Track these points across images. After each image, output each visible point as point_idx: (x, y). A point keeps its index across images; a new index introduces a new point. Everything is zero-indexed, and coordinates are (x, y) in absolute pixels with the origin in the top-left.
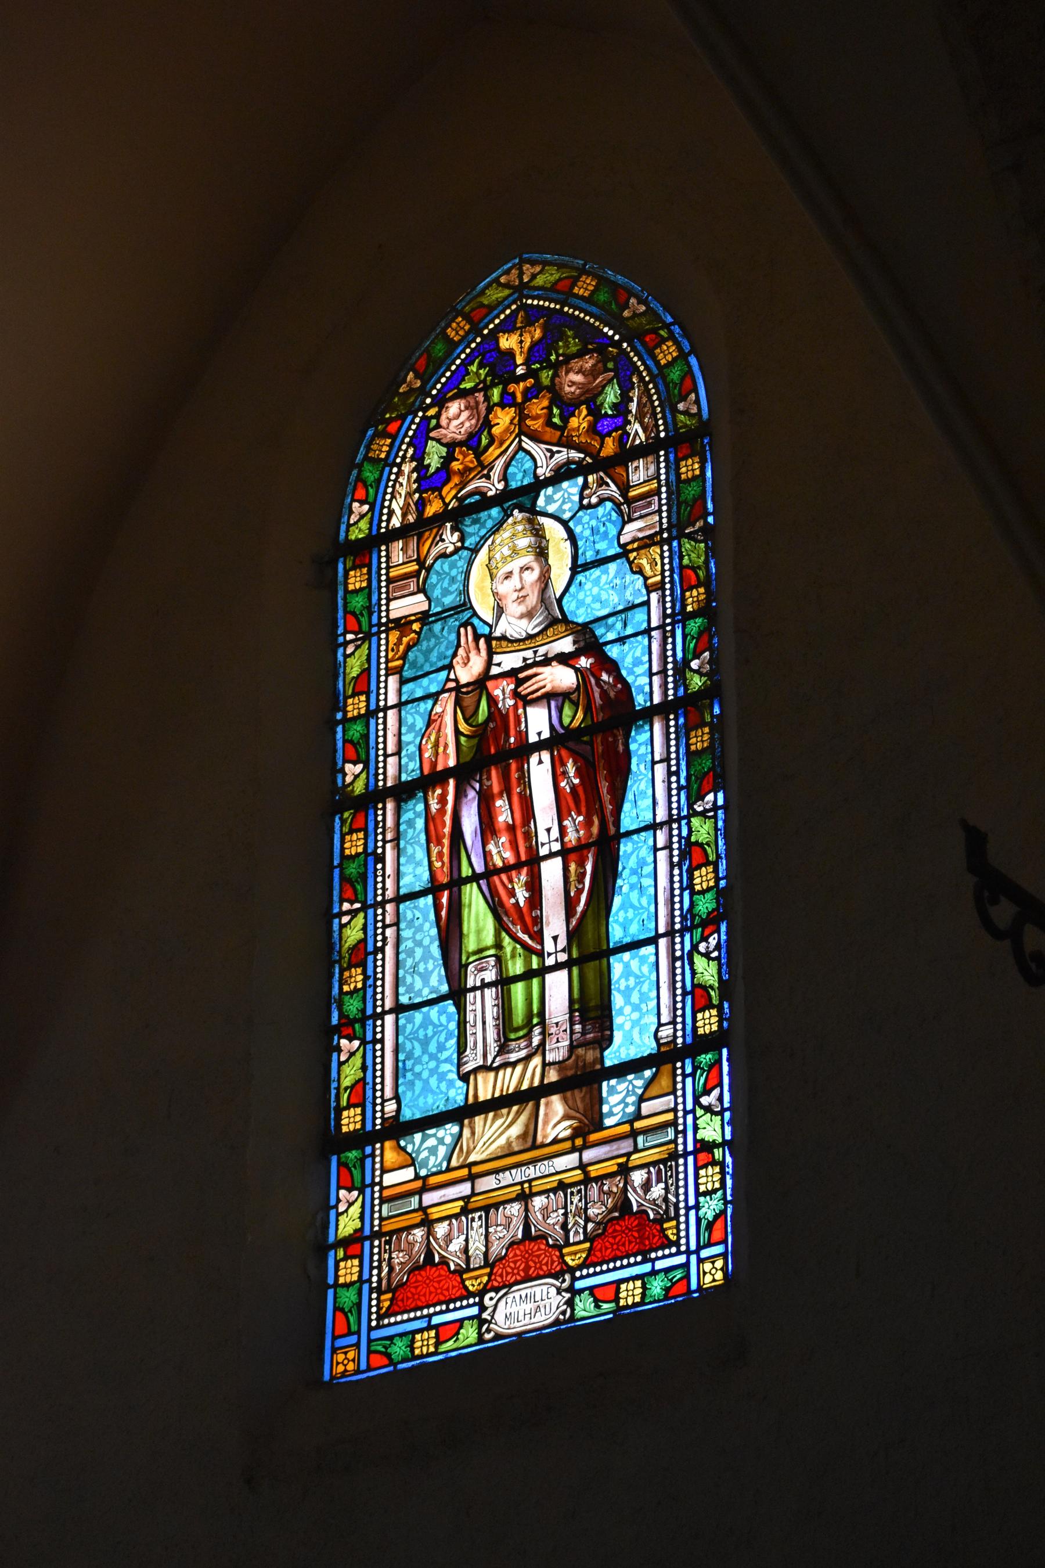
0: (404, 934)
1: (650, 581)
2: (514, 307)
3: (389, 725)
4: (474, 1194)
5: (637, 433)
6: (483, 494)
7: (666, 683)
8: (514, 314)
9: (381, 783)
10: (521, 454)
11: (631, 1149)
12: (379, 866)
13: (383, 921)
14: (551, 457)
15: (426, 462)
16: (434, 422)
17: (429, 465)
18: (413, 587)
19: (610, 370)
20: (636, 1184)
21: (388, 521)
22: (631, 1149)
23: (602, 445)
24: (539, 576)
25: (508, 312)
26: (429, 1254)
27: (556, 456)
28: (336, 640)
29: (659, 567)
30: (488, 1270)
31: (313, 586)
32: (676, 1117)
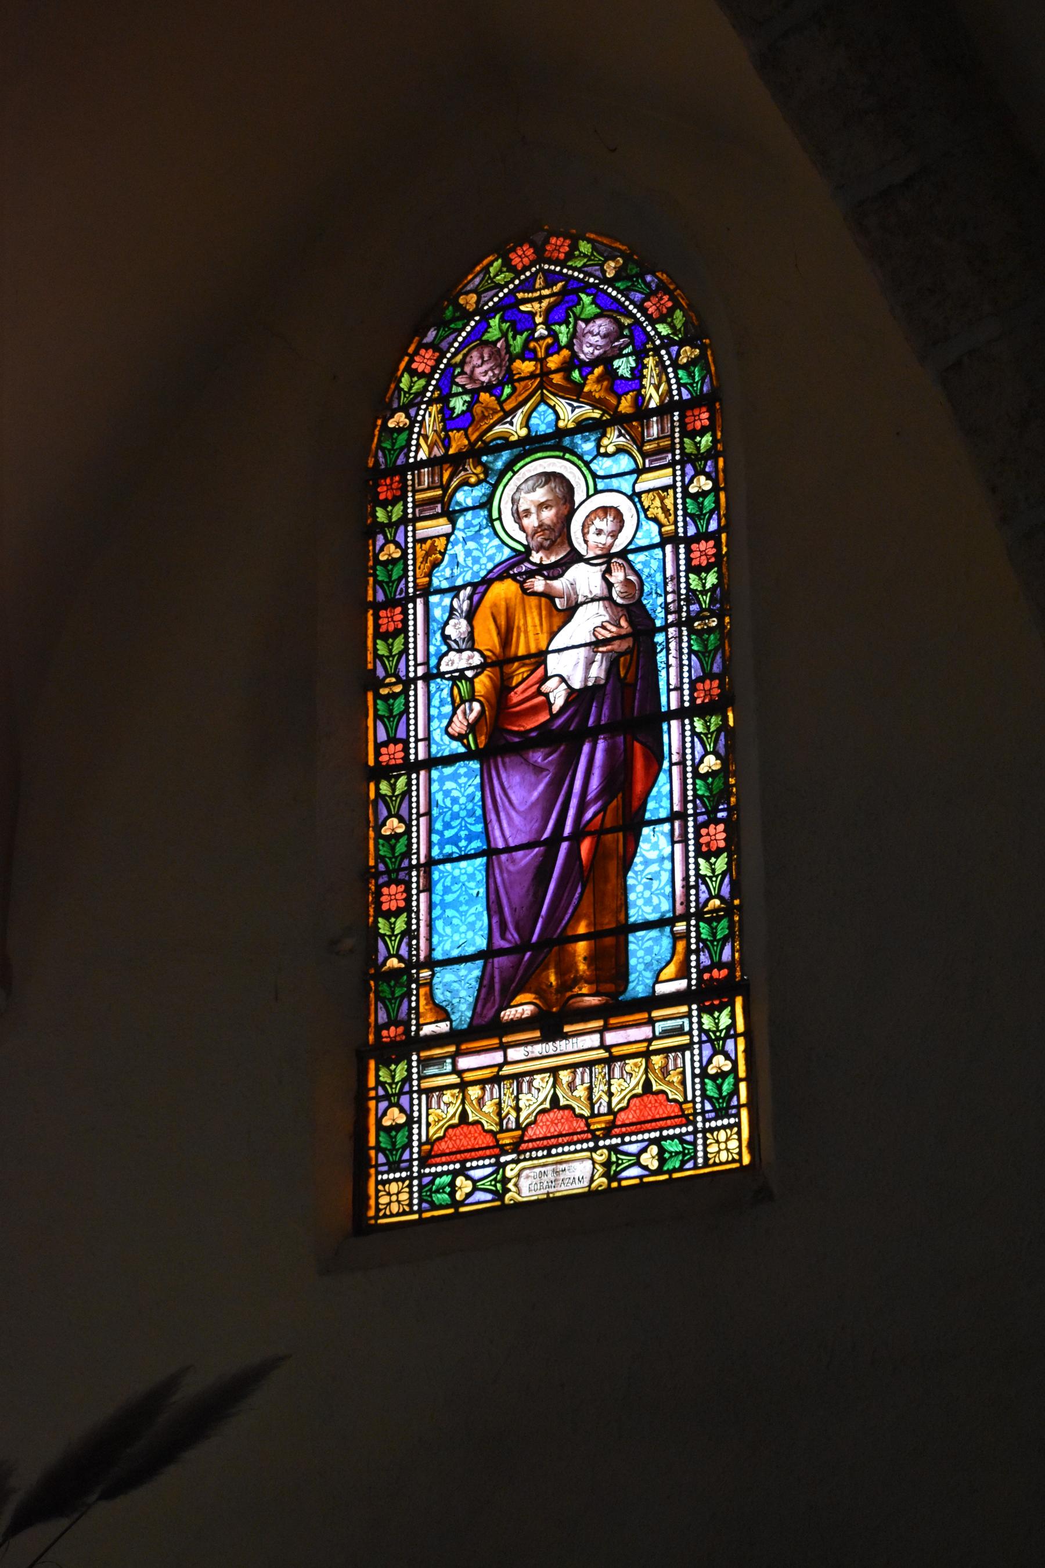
0: (436, 899)
1: (663, 530)
2: (534, 269)
3: (421, 917)
4: (506, 1062)
5: (651, 397)
6: (506, 439)
7: (687, 851)
8: (534, 276)
9: (412, 757)
10: (542, 408)
11: (651, 1035)
12: (414, 942)
13: (416, 736)
14: (573, 411)
15: (451, 405)
16: (458, 370)
17: (454, 408)
18: (439, 509)
19: (625, 336)
20: (656, 1067)
21: (417, 452)
22: (651, 1035)
23: (619, 403)
24: (559, 534)
25: (528, 274)
26: (464, 1115)
27: (577, 411)
28: (368, 1093)
29: (672, 518)
30: (519, 1132)
31: (346, 516)
32: (673, 444)
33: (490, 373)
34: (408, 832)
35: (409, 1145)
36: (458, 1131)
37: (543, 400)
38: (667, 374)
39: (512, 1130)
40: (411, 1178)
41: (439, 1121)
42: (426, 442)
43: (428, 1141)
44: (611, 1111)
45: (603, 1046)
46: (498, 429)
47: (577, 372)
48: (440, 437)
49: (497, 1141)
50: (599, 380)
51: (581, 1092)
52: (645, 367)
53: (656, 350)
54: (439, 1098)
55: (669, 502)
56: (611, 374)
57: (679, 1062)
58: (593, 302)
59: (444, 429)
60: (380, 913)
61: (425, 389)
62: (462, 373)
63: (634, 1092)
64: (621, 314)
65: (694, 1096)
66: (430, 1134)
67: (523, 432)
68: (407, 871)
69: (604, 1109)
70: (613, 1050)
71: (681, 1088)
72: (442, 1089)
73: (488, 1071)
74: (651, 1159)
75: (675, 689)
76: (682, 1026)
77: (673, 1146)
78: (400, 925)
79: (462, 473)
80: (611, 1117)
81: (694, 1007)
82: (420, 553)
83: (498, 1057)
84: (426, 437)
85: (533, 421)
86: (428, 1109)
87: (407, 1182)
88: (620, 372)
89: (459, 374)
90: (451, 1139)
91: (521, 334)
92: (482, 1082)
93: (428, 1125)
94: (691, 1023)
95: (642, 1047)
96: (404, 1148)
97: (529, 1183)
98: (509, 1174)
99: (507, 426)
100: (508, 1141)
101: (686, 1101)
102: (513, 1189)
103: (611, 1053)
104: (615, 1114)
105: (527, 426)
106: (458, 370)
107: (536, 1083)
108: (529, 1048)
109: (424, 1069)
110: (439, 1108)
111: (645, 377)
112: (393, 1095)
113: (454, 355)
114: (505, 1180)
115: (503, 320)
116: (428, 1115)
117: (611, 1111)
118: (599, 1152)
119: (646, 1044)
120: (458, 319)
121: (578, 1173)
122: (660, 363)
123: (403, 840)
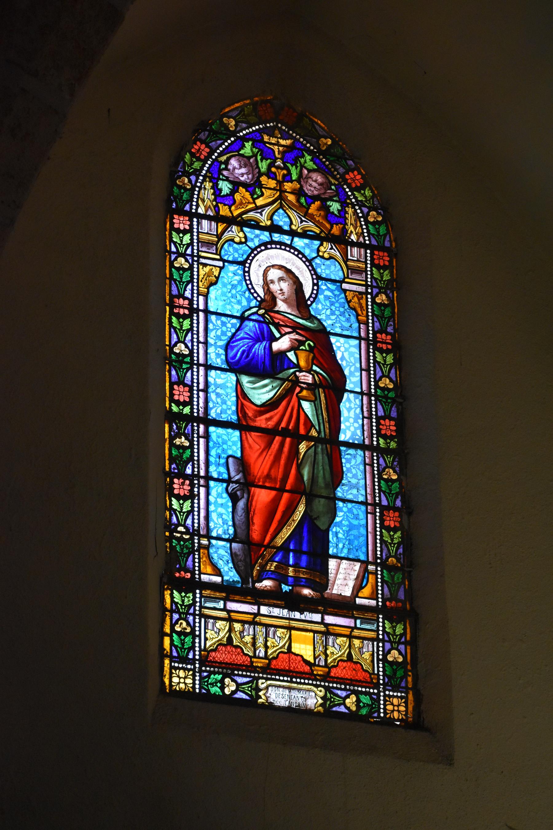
16: (223, 166)
27: (304, 223)
29: (365, 312)
33: (245, 176)
34: (191, 446)
35: (193, 648)
36: (345, 664)
37: (281, 207)
38: (360, 222)
39: (262, 658)
40: (194, 670)
41: (274, 646)
42: (204, 205)
43: (205, 649)
44: (326, 665)
45: (322, 622)
46: (251, 214)
47: (303, 198)
48: (212, 204)
49: (312, 671)
50: (319, 209)
51: (248, 639)
52: (347, 213)
53: (353, 206)
54: (214, 624)
55: (363, 302)
56: (325, 208)
57: (370, 646)
58: (311, 160)
59: (215, 200)
60: (172, 495)
61: (202, 168)
62: (226, 169)
63: (342, 658)
64: (330, 175)
65: (378, 671)
66: (207, 646)
67: (269, 223)
68: (181, 470)
69: (262, 654)
70: (232, 614)
71: (371, 664)
72: (216, 618)
73: (249, 616)
74: (351, 701)
75: (202, 390)
76: (361, 623)
77: (365, 699)
78: (187, 506)
79: (230, 233)
80: (327, 670)
81: (381, 616)
82: (202, 273)
83: (253, 609)
84: (203, 201)
85: (275, 217)
86: (205, 629)
87: (387, 698)
88: (331, 209)
89: (224, 169)
90: (219, 652)
91: (267, 160)
92: (243, 622)
93: (206, 639)
94: (200, 602)
95: (347, 631)
96: (189, 649)
97: (278, 695)
98: (262, 686)
99: (258, 215)
100: (259, 665)
101: (374, 673)
102: (263, 697)
103: (328, 629)
104: (330, 669)
105: (271, 218)
106: (223, 166)
107: (278, 633)
108: (271, 609)
109: (205, 602)
110: (274, 638)
111: (347, 219)
112: (395, 642)
113: (220, 155)
114: (258, 690)
115: (253, 146)
116: (205, 633)
117: (326, 665)
118: (319, 689)
119: (252, 616)
120: (224, 134)
121: (311, 698)
122: (355, 213)
123: (188, 452)
